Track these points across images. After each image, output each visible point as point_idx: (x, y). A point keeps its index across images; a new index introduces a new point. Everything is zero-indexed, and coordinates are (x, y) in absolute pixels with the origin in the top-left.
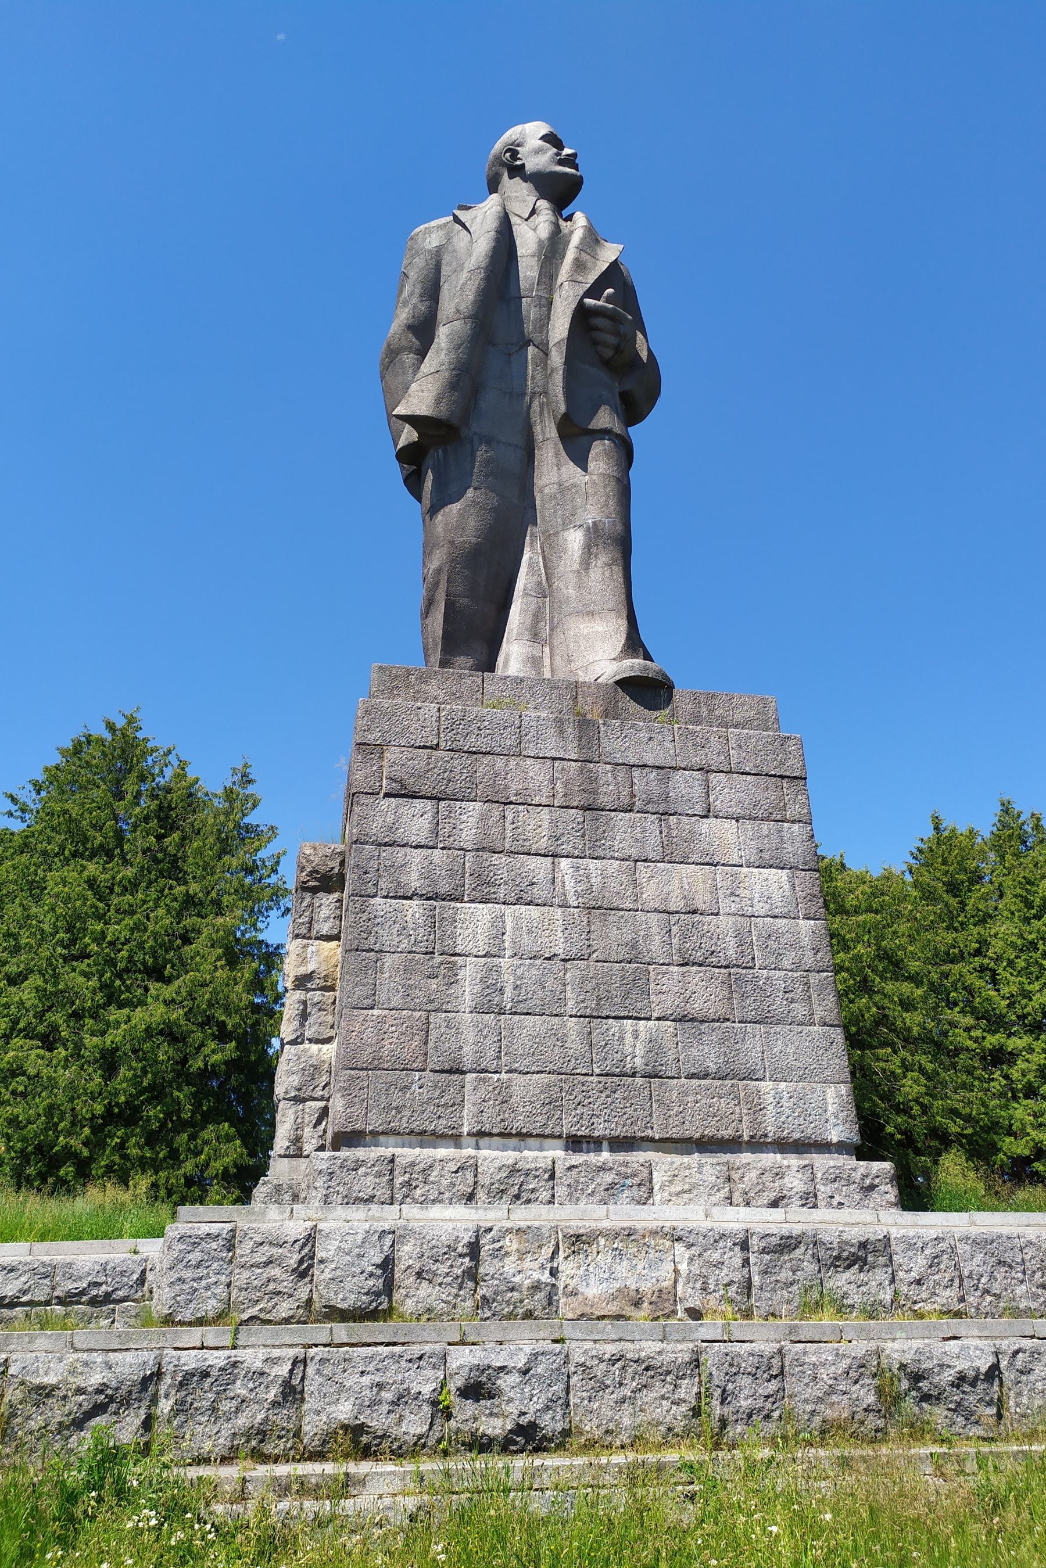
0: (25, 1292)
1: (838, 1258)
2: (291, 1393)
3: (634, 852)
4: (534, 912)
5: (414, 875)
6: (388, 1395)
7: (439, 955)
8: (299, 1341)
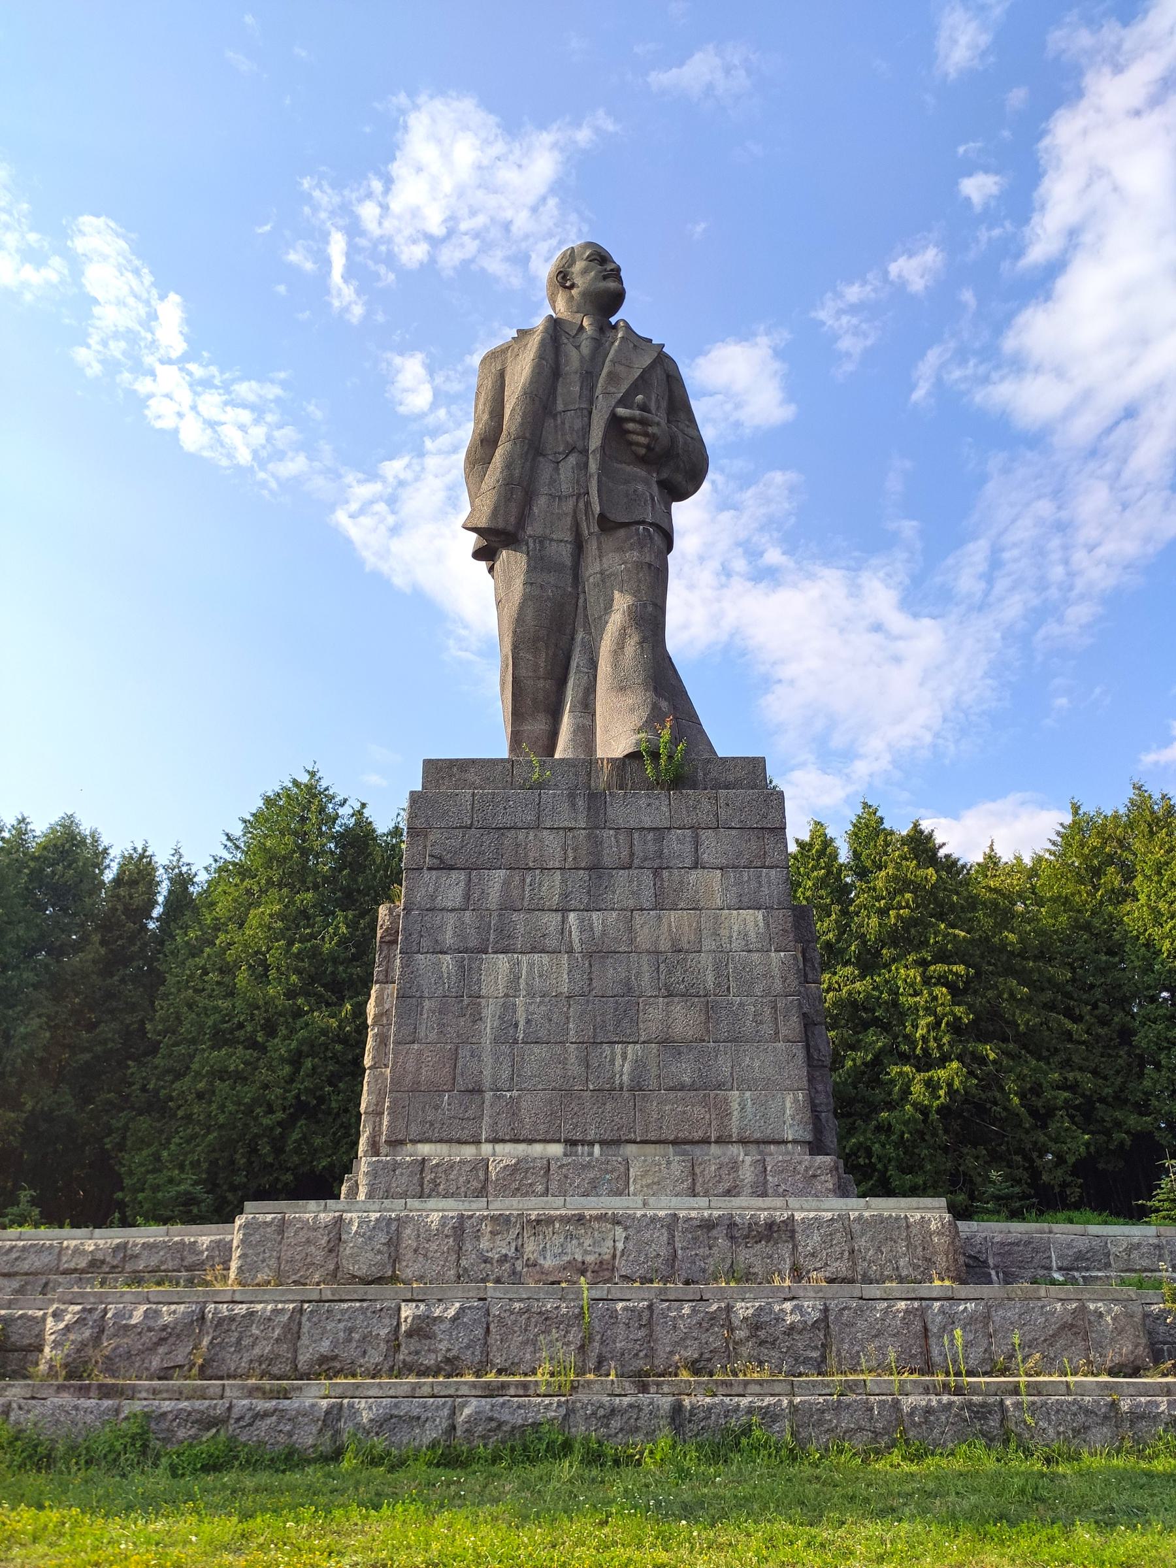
0: (162, 1263)
2: (293, 1332)
3: (631, 903)
4: (545, 958)
5: (449, 934)
6: (356, 1336)
7: (465, 998)
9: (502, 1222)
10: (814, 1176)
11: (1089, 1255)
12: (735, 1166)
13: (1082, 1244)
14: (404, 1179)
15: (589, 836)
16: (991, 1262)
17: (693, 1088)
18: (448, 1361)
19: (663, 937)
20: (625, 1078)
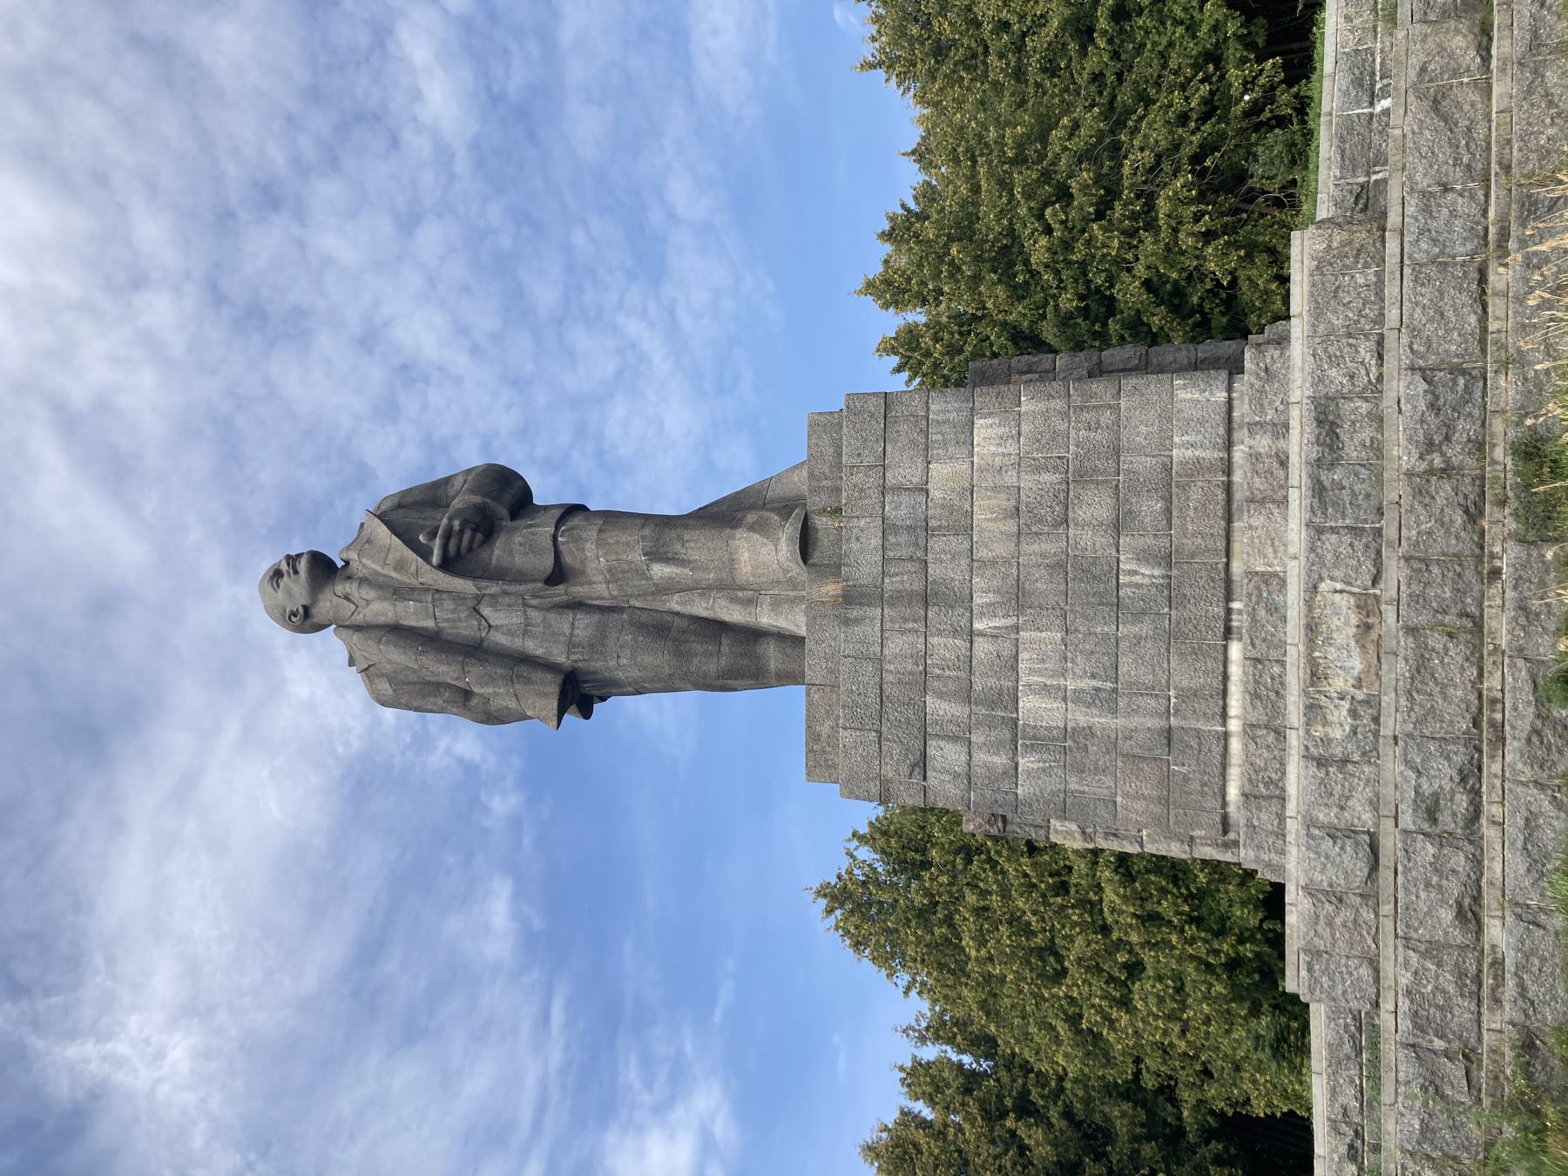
0: (1352, 1081)
1: (1331, 447)
2: (1432, 950)
3: (964, 562)
4: (1023, 656)
5: (996, 759)
6: (1435, 879)
7: (1066, 744)
8: (1391, 942)
9: (1313, 710)
10: (1267, 369)
11: (1357, 72)
12: (1255, 457)
13: (1343, 80)
14: (1264, 817)
15: (891, 605)
16: (1362, 179)
17: (1168, 499)
18: (1463, 780)
19: (1003, 528)
20: (1156, 572)
